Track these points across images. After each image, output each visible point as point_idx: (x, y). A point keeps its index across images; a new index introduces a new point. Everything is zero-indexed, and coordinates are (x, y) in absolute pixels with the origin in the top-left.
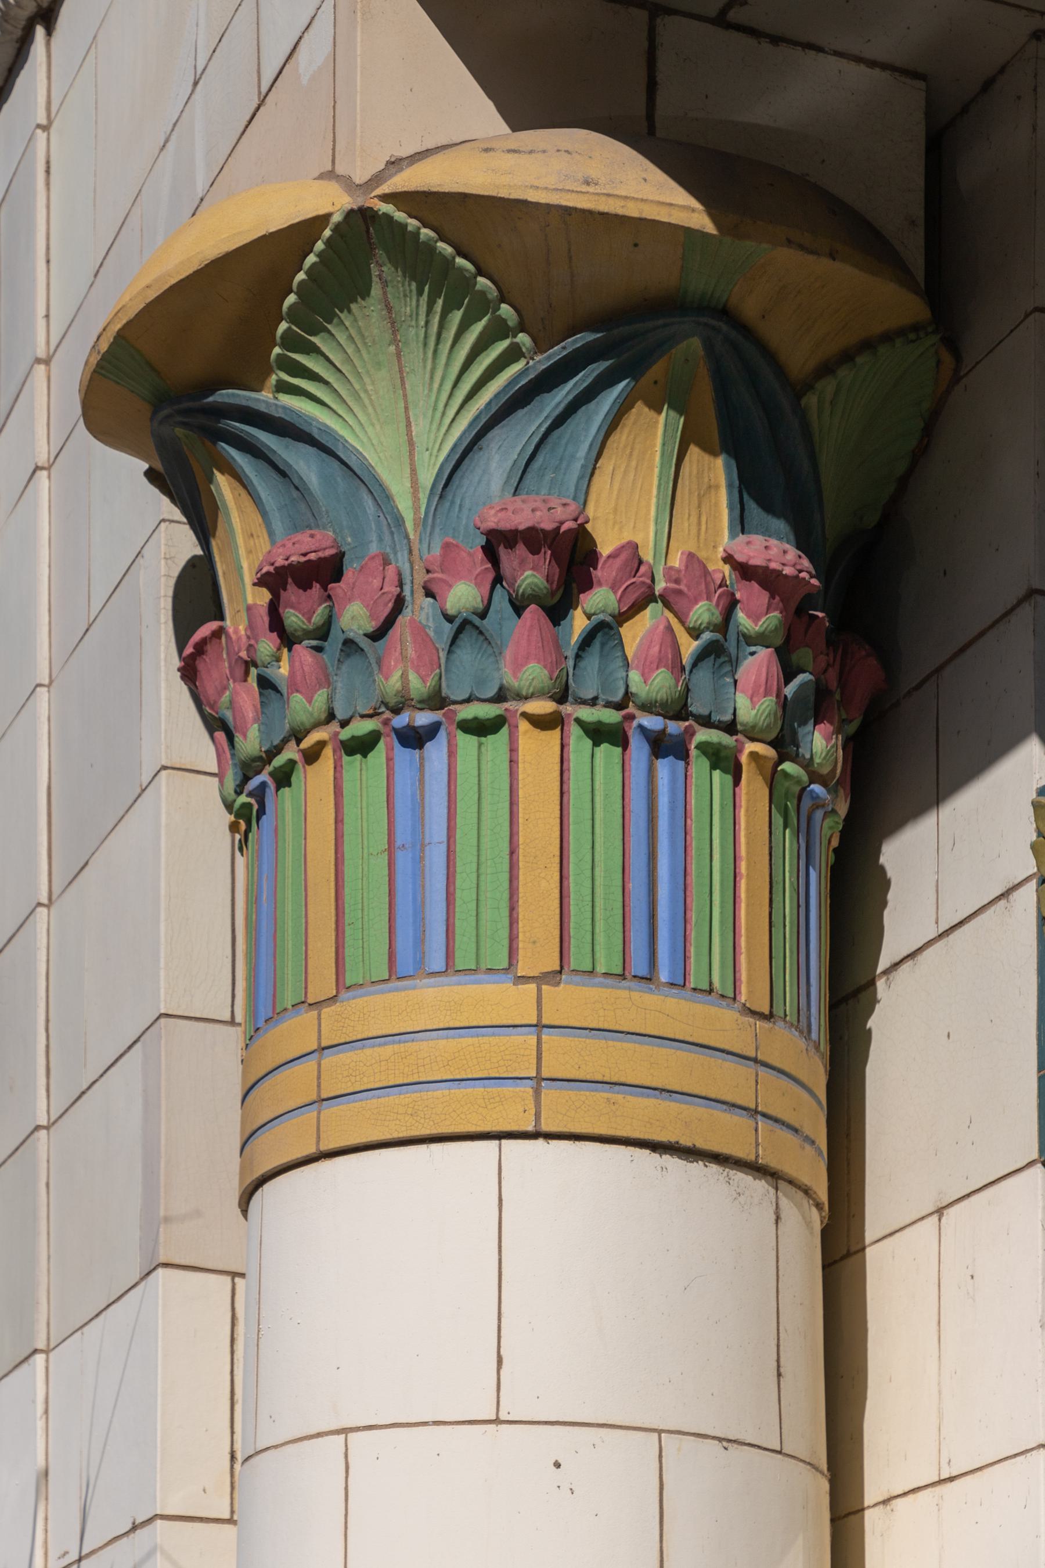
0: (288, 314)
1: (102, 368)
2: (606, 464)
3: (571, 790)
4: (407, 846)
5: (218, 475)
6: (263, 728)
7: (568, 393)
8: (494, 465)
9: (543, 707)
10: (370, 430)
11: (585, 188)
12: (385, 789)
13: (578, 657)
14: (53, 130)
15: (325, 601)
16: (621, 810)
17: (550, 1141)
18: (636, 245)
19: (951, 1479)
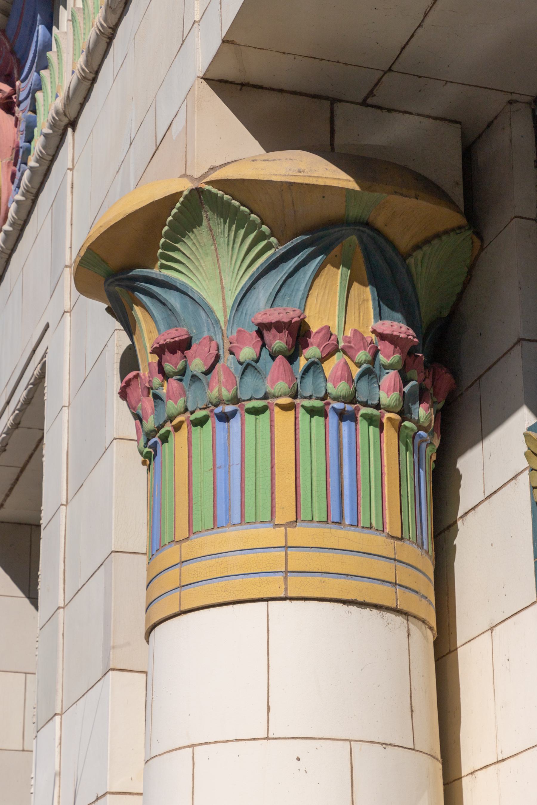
0: (165, 235)
1: (82, 263)
2: (314, 292)
3: (300, 438)
4: (222, 467)
5: (135, 307)
6: (155, 417)
7: (295, 262)
8: (261, 295)
9: (286, 400)
10: (203, 283)
11: (298, 174)
12: (211, 441)
13: (302, 378)
14: (74, 170)
15: (183, 359)
16: (325, 446)
17: (292, 601)
18: (324, 197)
19: (503, 760)
